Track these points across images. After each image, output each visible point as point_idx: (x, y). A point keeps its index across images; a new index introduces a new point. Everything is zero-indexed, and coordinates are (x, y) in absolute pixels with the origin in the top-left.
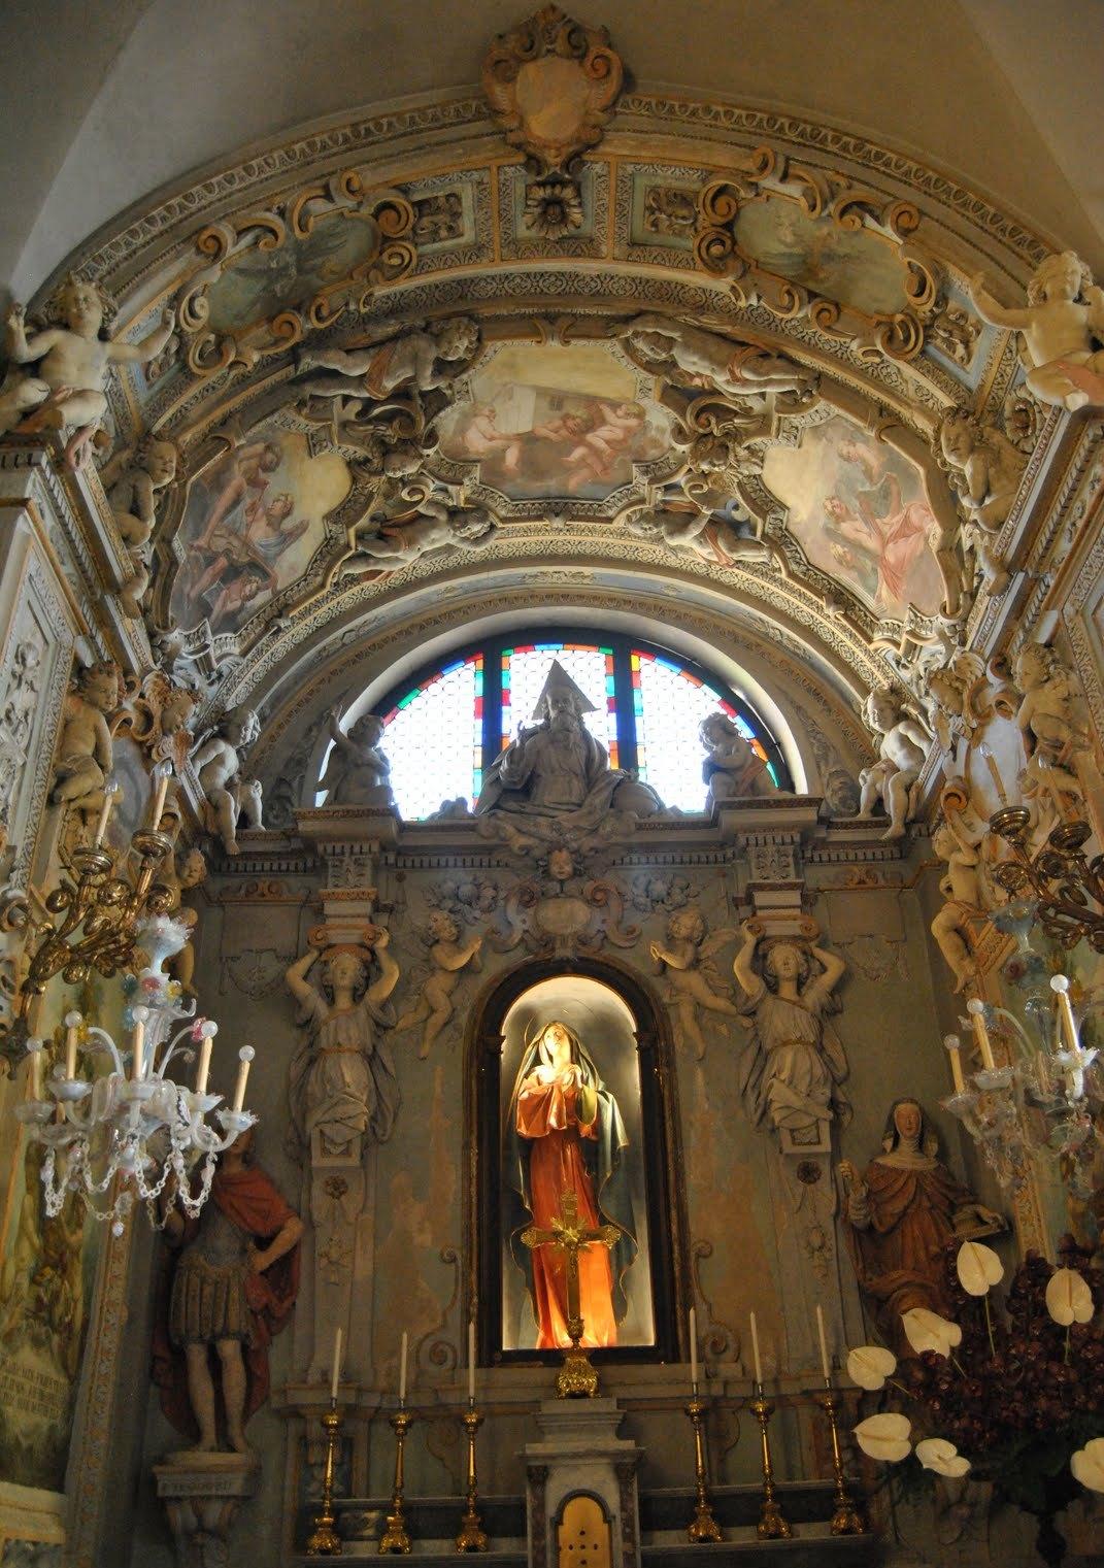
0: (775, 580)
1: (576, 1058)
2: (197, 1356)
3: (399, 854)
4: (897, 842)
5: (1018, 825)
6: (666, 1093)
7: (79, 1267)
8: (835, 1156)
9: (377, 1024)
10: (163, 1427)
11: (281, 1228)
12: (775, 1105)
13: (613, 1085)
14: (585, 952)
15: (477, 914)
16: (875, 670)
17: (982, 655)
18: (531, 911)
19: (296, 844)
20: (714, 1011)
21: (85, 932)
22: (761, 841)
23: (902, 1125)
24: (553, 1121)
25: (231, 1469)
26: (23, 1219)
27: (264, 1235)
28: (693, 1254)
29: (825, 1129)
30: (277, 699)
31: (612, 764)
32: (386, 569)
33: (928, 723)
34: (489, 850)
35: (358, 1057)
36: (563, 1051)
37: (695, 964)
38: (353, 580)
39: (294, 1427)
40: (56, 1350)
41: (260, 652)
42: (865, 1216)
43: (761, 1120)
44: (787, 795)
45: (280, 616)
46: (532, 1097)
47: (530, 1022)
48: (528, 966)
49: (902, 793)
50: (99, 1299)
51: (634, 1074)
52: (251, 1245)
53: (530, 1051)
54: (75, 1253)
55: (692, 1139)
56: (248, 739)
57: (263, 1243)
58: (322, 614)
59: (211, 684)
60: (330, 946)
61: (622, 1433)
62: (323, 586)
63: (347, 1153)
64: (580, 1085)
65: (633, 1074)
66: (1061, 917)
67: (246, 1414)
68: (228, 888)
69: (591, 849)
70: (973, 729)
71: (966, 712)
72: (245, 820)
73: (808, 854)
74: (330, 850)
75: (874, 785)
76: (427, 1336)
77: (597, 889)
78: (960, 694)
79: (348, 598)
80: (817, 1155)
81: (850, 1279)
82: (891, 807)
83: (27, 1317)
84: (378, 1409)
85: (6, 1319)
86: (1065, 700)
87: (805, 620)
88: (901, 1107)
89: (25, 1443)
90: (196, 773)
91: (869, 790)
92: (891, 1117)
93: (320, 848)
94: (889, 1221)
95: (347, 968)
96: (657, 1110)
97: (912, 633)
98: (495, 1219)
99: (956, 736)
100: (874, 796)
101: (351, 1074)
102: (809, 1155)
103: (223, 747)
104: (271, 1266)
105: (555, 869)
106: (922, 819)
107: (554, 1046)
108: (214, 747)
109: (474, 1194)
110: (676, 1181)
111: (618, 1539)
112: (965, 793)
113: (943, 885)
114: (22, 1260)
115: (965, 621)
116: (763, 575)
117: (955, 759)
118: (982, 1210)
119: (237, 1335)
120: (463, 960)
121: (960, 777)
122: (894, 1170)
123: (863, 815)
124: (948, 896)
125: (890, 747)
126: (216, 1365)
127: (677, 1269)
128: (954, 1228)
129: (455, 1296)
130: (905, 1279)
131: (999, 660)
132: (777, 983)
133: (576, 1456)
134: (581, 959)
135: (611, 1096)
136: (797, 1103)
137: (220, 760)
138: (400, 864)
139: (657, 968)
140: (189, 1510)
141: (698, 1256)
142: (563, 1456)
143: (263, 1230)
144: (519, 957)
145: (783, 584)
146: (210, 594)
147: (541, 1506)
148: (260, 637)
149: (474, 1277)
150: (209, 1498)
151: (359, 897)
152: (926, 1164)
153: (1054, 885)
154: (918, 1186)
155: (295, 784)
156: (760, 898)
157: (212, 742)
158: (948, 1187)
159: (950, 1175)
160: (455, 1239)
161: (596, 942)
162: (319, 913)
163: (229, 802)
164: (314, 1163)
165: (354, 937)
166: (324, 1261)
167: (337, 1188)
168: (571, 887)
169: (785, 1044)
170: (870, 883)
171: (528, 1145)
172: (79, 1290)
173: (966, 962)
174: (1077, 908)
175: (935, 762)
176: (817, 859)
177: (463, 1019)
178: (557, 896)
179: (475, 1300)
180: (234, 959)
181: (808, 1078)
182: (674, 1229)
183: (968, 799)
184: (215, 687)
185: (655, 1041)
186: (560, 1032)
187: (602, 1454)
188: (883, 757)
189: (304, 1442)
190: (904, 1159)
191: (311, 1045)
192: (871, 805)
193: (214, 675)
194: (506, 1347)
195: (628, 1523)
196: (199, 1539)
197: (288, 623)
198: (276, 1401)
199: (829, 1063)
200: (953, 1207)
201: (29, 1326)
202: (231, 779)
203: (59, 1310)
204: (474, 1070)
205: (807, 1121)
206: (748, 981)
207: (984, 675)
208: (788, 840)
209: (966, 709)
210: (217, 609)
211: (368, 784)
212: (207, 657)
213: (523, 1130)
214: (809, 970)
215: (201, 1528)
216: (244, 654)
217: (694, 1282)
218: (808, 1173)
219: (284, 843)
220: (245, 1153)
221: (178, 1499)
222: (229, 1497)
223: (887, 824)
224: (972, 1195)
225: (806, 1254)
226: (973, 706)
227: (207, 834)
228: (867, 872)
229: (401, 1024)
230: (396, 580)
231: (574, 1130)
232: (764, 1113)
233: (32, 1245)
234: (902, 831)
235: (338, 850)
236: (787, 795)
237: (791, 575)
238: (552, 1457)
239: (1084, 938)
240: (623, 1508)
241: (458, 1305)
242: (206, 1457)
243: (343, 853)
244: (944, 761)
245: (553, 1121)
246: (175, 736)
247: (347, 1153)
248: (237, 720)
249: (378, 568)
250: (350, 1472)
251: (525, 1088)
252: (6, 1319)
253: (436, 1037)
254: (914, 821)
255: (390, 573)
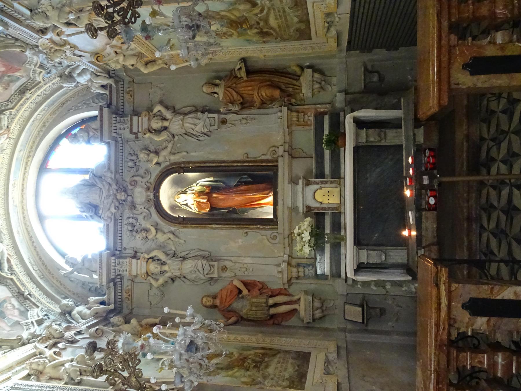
0: (15, 115)
1: (185, 192)
2: (273, 311)
3: (116, 250)
4: (117, 82)
5: (93, 28)
6: (198, 165)
7: (245, 353)
8: (218, 112)
9: (174, 256)
10: (293, 321)
11: (236, 286)
12: (203, 130)
13: (195, 181)
14: (152, 189)
15: (138, 224)
16: (53, 82)
17: (39, 39)
18: (137, 206)
19: (112, 284)
20: (172, 148)
21: (124, 371)
22: (115, 128)
23: (210, 91)
24: (205, 201)
25: (305, 300)
26: (227, 376)
27: (238, 291)
28: (248, 159)
29: (211, 115)
30: (58, 293)
31: (87, 177)
32: (6, 256)
33: (72, 65)
34: (116, 220)
35: (183, 263)
36: (183, 197)
37: (157, 153)
38: (10, 267)
39: (293, 281)
40: (270, 359)
41: (38, 301)
42: (238, 105)
43: (208, 136)
44: (98, 118)
45: (23, 295)
46: (197, 207)
47: (174, 207)
48: (156, 208)
49: (98, 77)
50: (255, 344)
51: (191, 175)
52: (240, 296)
53: (184, 207)
54: (241, 354)
55: (212, 157)
56: (72, 303)
57: (240, 291)
58: (25, 279)
59: (49, 318)
60: (147, 273)
61: (297, 184)
62: (12, 279)
63: (213, 266)
64: (194, 192)
65: (191, 175)
66: (128, 17)
67: (289, 295)
68: (127, 307)
69: (116, 185)
70: (71, 47)
71: (64, 49)
72: (103, 303)
73: (121, 113)
74: (114, 274)
75: (96, 88)
76: (268, 241)
77: (131, 184)
78: (57, 50)
79: (18, 269)
80: (218, 118)
81: (255, 111)
82: (105, 82)
83: (259, 371)
84: (289, 256)
85: (259, 379)
86: (53, 8)
87: (33, 106)
88: (204, 90)
89: (297, 368)
90: (84, 321)
91: (98, 89)
92: (207, 93)
93: (113, 277)
94: (239, 98)
95: (153, 267)
96: (202, 168)
97: (35, 66)
98: (234, 220)
99: (74, 54)
100: (101, 88)
101: (188, 266)
102: (218, 121)
103: (74, 312)
104: (247, 289)
105: (123, 198)
106: (110, 74)
107: (181, 199)
108: (74, 315)
109: (227, 226)
110: (216, 163)
111: (326, 185)
112: (96, 54)
113: (131, 67)
114: (241, 375)
115: (28, 44)
116: (13, 118)
117: (83, 56)
118: (236, 69)
119: (267, 299)
120: (153, 230)
121: (91, 56)
122: (224, 95)
123: (107, 92)
124: (135, 66)
125: (83, 80)
126: (275, 305)
127: (251, 164)
128: (242, 77)
129: (258, 232)
130: (257, 94)
131: (40, 32)
132: (164, 127)
133: (303, 197)
134: (154, 190)
135: (198, 182)
136: (202, 123)
137: (79, 313)
138: (120, 249)
139: (157, 166)
140: (316, 312)
141: (248, 158)
142: (303, 201)
143: (236, 292)
144: (153, 210)
145: (18, 111)
146: (9, 322)
147: (318, 208)
148: (31, 302)
149: (252, 227)
150: (313, 306)
151: (131, 263)
152: (222, 83)
153: (117, 18)
154: (229, 87)
155: (91, 285)
156: (135, 130)
157: (73, 317)
158: (230, 78)
159: (226, 76)
160: (241, 232)
161: (148, 185)
162: (136, 276)
163: (95, 309)
164: (217, 276)
165: (144, 264)
166: (246, 272)
167: (224, 269)
168: (130, 192)
169: (183, 126)
170: (131, 93)
171: (212, 208)
172: (252, 352)
173: (158, 63)
174: (125, 11)
175: (86, 64)
176: (122, 110)
177: (173, 229)
178: (133, 198)
179: (258, 226)
180: (151, 304)
181: (194, 119)
182: (239, 164)
183: (98, 54)
184: (50, 316)
185: (181, 167)
186: (177, 197)
187: (303, 190)
188: (86, 83)
189: (298, 278)
190: (220, 91)
191: (179, 278)
192: (103, 89)
193: (46, 317)
194: (272, 217)
195: (322, 183)
196: (324, 308)
197: (27, 291)
198: (286, 286)
199: (190, 112)
200: (236, 77)
201: (262, 370)
202: (87, 308)
203: (258, 359)
204: (189, 225)
205: (208, 120)
206: (163, 136)
207: (47, 39)
208: (115, 119)
209: (62, 49)
210: (16, 319)
211: (90, 260)
212: (36, 321)
213: (208, 210)
214: (160, 116)
215: (321, 308)
216: (38, 307)
217: (255, 159)
218: (224, 122)
219: (111, 288)
220: (213, 298)
221: (313, 315)
222: (313, 300)
223: (111, 86)
224: (233, 71)
225: (248, 124)
226: (61, 46)
227: (106, 316)
228: (128, 93)
229: (174, 249)
230: (12, 252)
231: (207, 194)
232: (205, 134)
233: (237, 371)
234: (112, 80)
235: (114, 271)
236: (98, 118)
237: (12, 108)
238: (303, 204)
239: (136, 9)
240: (318, 184)
241: (260, 231)
242: (301, 308)
243: (115, 269)
244: (85, 61)
245: (205, 201)
246: (65, 332)
247: (213, 266)
248: (65, 308)
249: (5, 259)
250: (307, 264)
251: (195, 209)
252: (259, 379)
253: (179, 238)
254: (109, 75)
255: (8, 254)
